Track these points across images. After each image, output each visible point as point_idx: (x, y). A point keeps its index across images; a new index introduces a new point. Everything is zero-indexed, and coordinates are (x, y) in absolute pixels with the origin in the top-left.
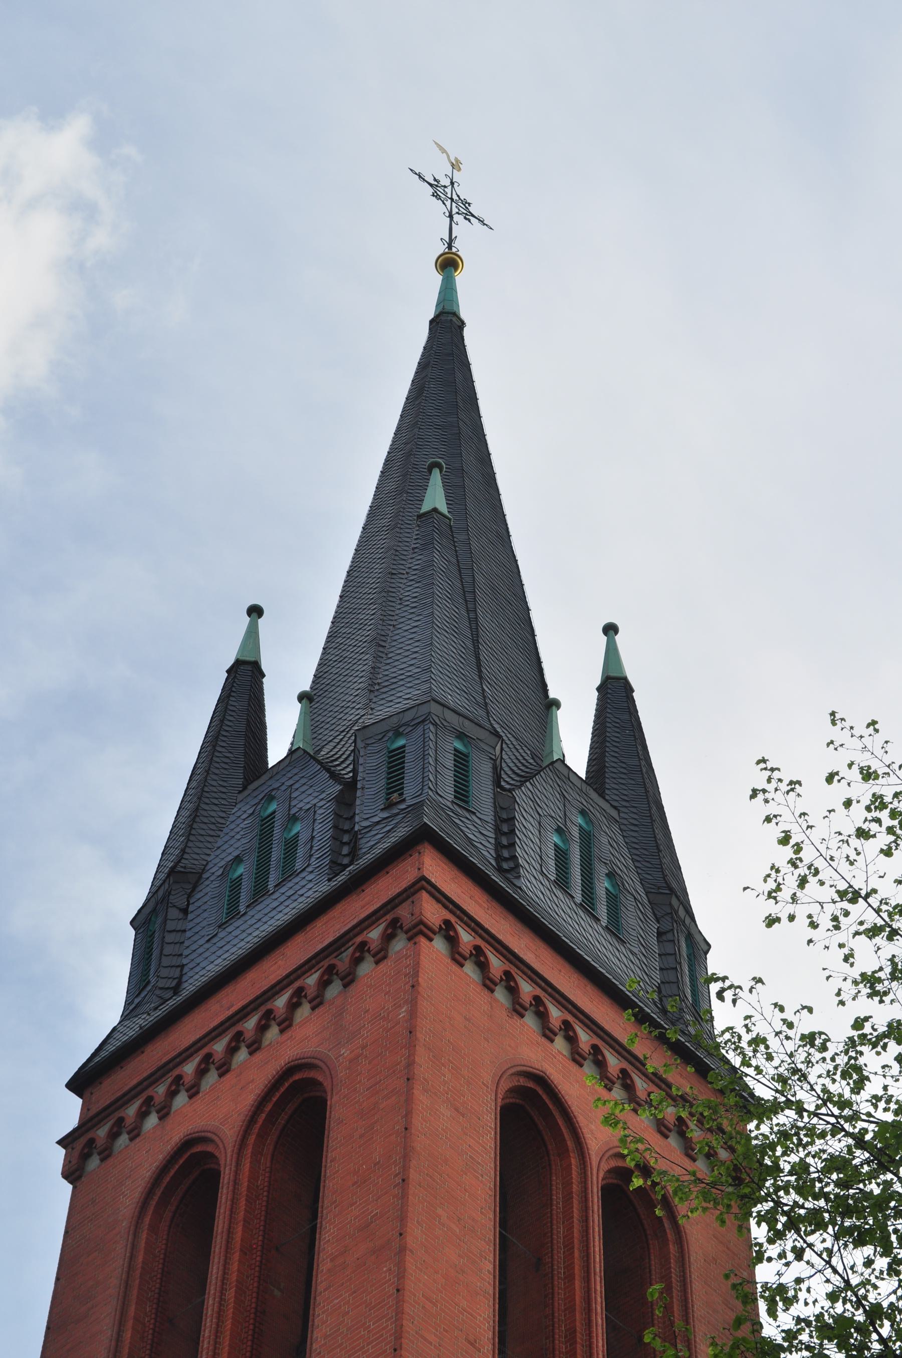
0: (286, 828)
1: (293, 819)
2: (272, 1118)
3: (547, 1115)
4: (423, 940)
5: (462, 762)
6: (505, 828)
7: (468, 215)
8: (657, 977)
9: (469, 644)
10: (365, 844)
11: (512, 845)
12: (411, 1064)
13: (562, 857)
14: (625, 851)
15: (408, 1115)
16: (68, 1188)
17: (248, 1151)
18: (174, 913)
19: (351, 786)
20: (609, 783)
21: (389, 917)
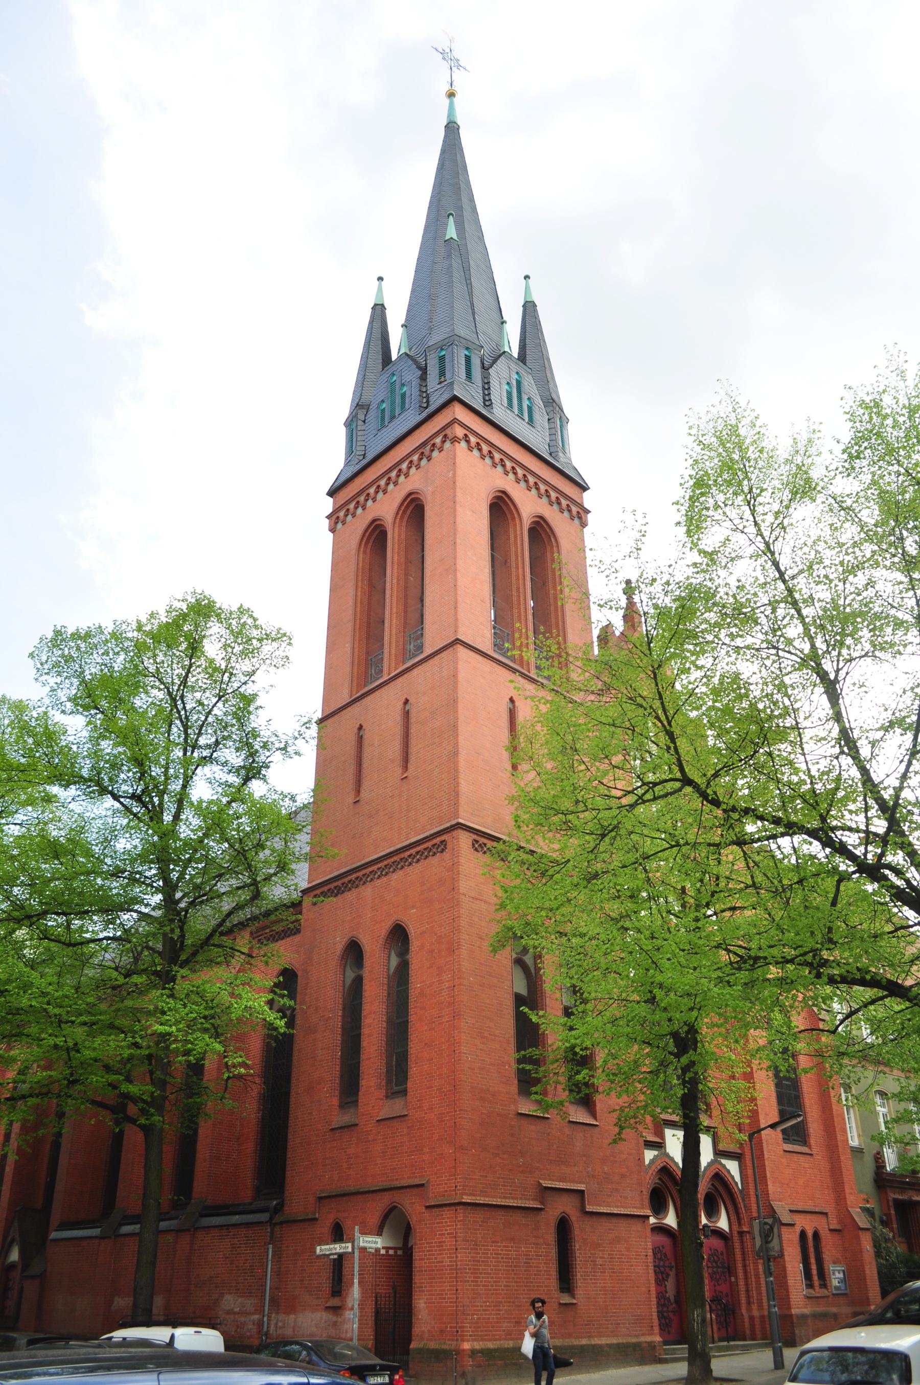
0: (401, 389)
1: (403, 385)
2: (405, 512)
3: (507, 505)
4: (456, 444)
5: (468, 359)
6: (487, 398)
7: (459, 66)
8: (548, 440)
9: (469, 303)
10: (432, 399)
11: (489, 394)
12: (455, 496)
13: (509, 394)
14: (535, 387)
15: (455, 517)
16: (331, 535)
17: (397, 525)
18: (360, 423)
19: (424, 370)
20: (528, 358)
21: (443, 433)
